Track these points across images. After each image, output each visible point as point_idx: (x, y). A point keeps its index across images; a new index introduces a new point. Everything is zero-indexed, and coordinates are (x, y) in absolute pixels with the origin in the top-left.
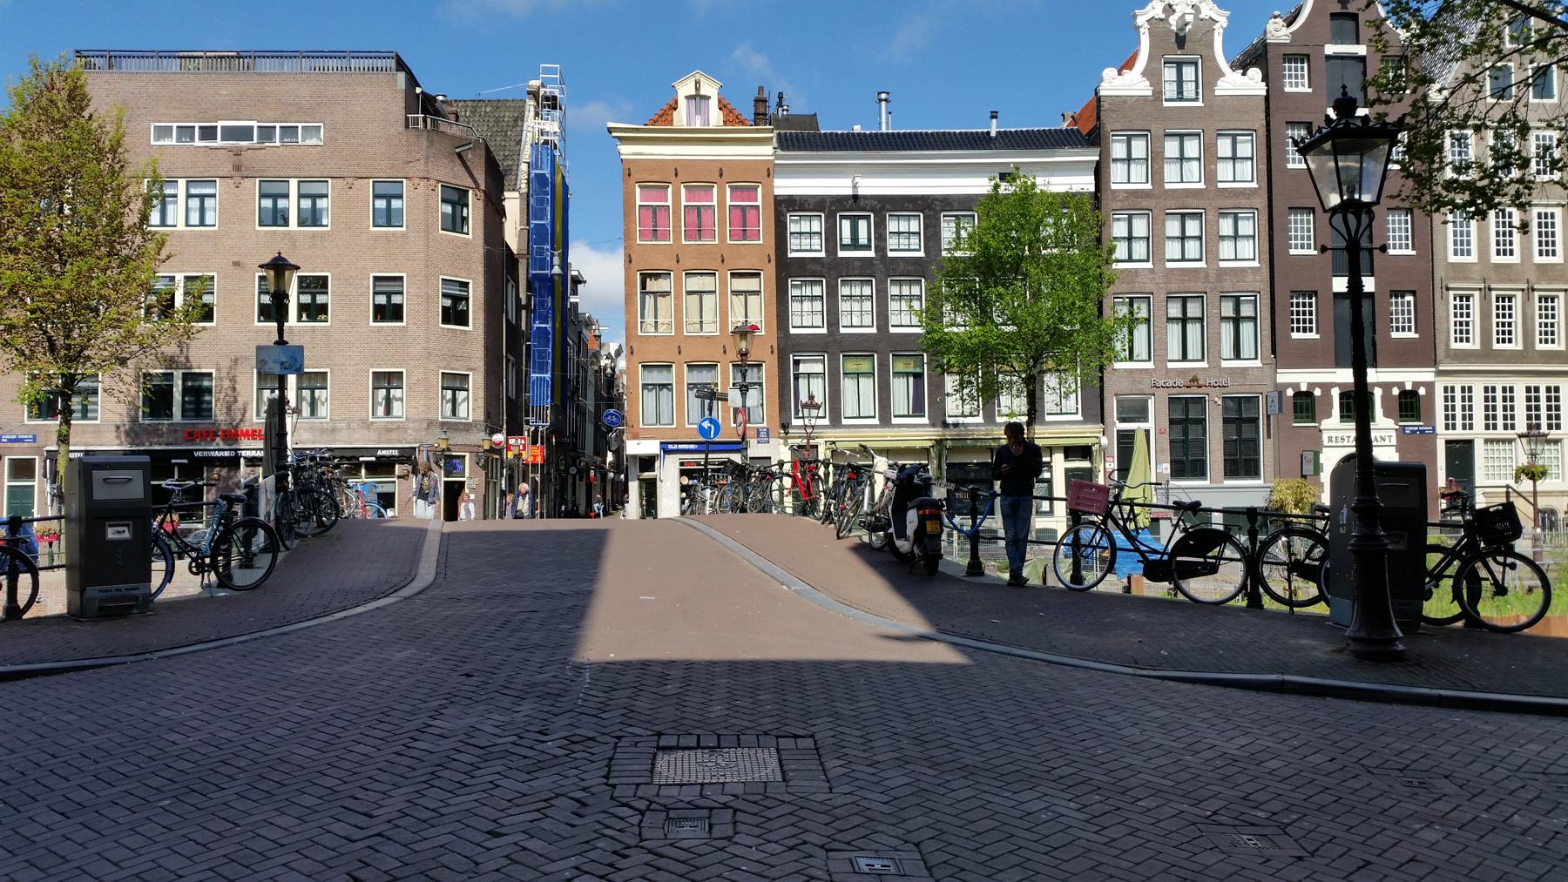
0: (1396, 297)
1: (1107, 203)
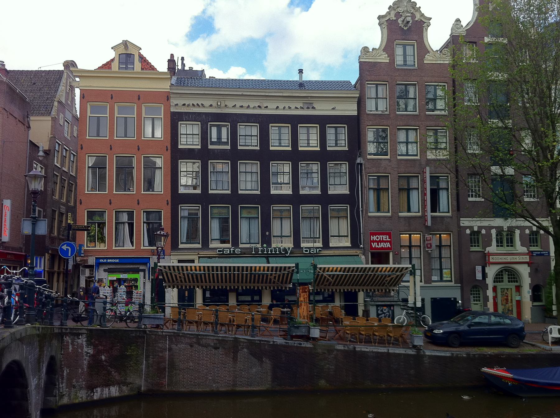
0: (471, 177)
1: (364, 121)
